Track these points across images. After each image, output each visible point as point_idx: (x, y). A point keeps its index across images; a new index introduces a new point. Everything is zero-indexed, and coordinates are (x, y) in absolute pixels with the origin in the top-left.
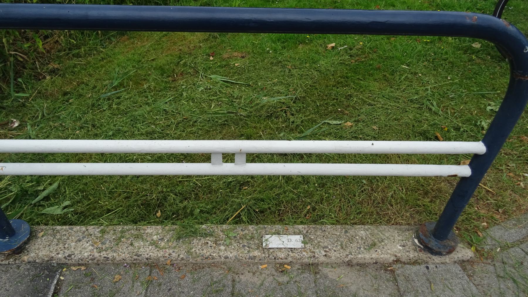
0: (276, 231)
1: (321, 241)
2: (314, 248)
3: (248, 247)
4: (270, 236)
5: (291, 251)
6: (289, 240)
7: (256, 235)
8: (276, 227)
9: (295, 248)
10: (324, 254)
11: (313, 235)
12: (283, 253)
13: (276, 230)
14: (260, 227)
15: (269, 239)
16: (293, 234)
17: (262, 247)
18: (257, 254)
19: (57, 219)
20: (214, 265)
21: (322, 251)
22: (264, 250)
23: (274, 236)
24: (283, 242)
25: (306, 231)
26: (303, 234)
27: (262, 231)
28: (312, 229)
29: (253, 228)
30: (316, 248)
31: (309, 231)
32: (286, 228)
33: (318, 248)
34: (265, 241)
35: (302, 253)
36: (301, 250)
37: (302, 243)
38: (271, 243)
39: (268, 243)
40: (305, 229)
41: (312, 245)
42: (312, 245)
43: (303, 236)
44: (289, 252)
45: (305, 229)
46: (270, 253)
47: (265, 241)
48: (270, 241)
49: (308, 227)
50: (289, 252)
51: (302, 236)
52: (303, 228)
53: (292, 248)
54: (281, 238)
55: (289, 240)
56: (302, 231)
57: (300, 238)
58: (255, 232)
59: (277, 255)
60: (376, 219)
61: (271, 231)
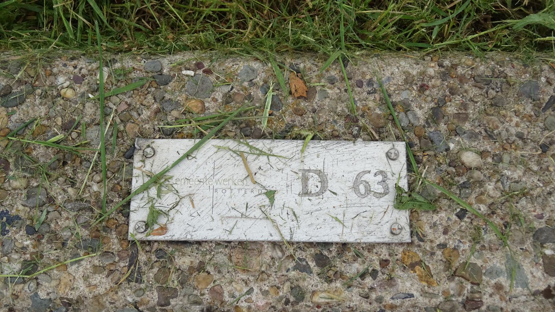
0: (234, 108)
1: (530, 181)
2: (476, 240)
3: (31, 231)
4: (185, 145)
5: (321, 261)
6: (313, 184)
7: (93, 133)
8: (230, 77)
9: (344, 246)
10: (542, 287)
11: (473, 136)
12: (262, 275)
13: (228, 99)
14: (125, 73)
15: (176, 173)
16: (340, 126)
17: (123, 236)
18: (82, 288)
19: (403, 39)
20: (167, 8)
21: (527, 266)
22: (133, 260)
23: (212, 144)
24: (271, 194)
25: (427, 106)
26: (411, 127)
27: (136, 101)
28: (473, 92)
29: (78, 80)
30: (489, 237)
31: (451, 109)
32: (297, 84)
33: (503, 236)
34: (145, 188)
35: (391, 281)
36: (384, 253)
37: (399, 203)
38: (185, 207)
39: (168, 200)
40: (423, 88)
41: (461, 215)
42: (461, 215)
43: (409, 145)
44: (306, 269)
45: (423, 88)
46: (173, 281)
47: (145, 188)
48: (184, 190)
49: (445, 75)
50: (306, 269)
51: (401, 147)
52: (409, 81)
53: (326, 245)
54: (255, 163)
55: (313, 184)
56: (407, 108)
57: (382, 164)
58: (89, 109)
59: (217, 293)
60: (124, 34)
61: (193, 104)
